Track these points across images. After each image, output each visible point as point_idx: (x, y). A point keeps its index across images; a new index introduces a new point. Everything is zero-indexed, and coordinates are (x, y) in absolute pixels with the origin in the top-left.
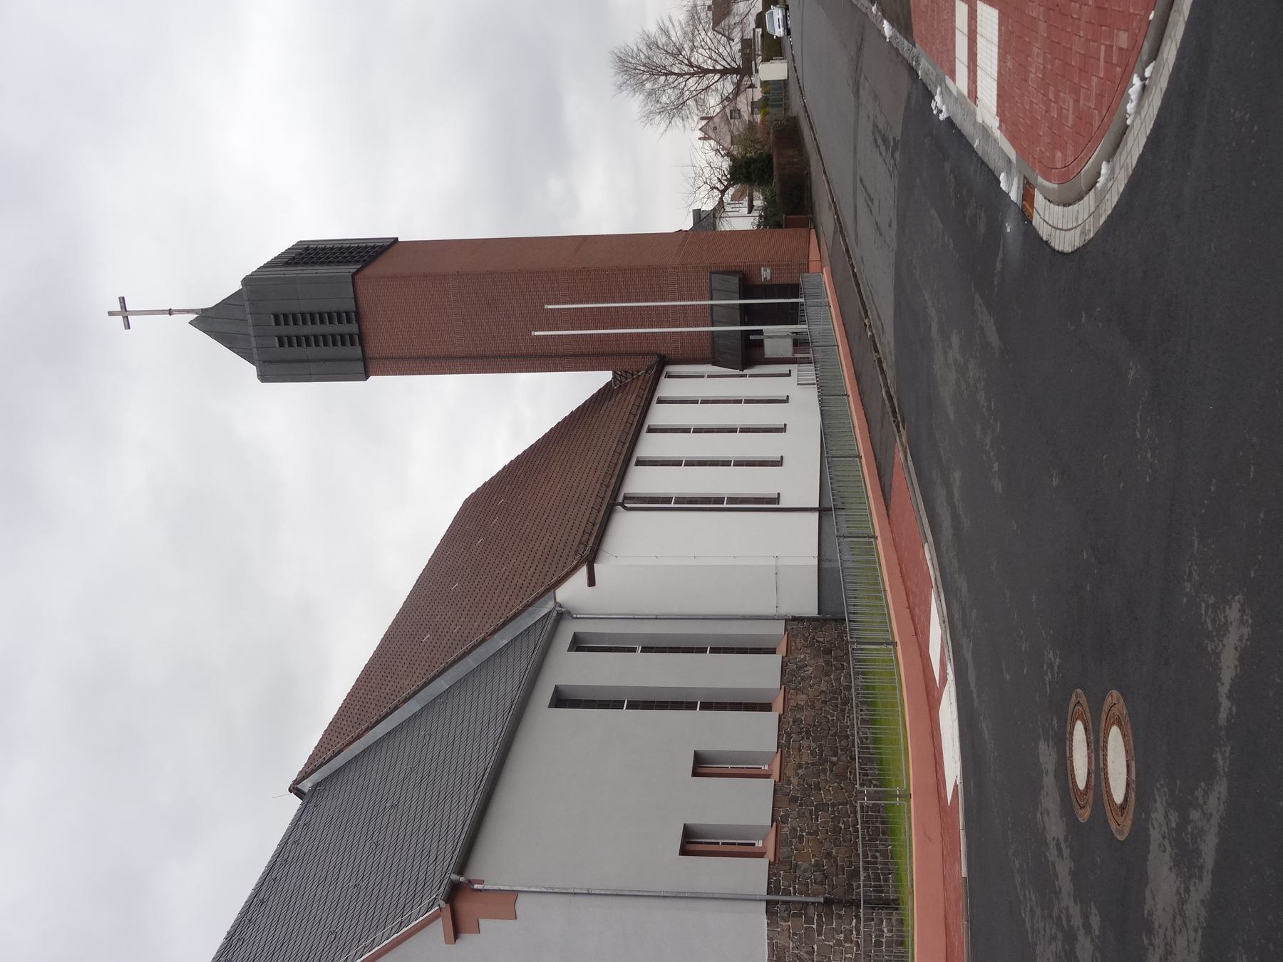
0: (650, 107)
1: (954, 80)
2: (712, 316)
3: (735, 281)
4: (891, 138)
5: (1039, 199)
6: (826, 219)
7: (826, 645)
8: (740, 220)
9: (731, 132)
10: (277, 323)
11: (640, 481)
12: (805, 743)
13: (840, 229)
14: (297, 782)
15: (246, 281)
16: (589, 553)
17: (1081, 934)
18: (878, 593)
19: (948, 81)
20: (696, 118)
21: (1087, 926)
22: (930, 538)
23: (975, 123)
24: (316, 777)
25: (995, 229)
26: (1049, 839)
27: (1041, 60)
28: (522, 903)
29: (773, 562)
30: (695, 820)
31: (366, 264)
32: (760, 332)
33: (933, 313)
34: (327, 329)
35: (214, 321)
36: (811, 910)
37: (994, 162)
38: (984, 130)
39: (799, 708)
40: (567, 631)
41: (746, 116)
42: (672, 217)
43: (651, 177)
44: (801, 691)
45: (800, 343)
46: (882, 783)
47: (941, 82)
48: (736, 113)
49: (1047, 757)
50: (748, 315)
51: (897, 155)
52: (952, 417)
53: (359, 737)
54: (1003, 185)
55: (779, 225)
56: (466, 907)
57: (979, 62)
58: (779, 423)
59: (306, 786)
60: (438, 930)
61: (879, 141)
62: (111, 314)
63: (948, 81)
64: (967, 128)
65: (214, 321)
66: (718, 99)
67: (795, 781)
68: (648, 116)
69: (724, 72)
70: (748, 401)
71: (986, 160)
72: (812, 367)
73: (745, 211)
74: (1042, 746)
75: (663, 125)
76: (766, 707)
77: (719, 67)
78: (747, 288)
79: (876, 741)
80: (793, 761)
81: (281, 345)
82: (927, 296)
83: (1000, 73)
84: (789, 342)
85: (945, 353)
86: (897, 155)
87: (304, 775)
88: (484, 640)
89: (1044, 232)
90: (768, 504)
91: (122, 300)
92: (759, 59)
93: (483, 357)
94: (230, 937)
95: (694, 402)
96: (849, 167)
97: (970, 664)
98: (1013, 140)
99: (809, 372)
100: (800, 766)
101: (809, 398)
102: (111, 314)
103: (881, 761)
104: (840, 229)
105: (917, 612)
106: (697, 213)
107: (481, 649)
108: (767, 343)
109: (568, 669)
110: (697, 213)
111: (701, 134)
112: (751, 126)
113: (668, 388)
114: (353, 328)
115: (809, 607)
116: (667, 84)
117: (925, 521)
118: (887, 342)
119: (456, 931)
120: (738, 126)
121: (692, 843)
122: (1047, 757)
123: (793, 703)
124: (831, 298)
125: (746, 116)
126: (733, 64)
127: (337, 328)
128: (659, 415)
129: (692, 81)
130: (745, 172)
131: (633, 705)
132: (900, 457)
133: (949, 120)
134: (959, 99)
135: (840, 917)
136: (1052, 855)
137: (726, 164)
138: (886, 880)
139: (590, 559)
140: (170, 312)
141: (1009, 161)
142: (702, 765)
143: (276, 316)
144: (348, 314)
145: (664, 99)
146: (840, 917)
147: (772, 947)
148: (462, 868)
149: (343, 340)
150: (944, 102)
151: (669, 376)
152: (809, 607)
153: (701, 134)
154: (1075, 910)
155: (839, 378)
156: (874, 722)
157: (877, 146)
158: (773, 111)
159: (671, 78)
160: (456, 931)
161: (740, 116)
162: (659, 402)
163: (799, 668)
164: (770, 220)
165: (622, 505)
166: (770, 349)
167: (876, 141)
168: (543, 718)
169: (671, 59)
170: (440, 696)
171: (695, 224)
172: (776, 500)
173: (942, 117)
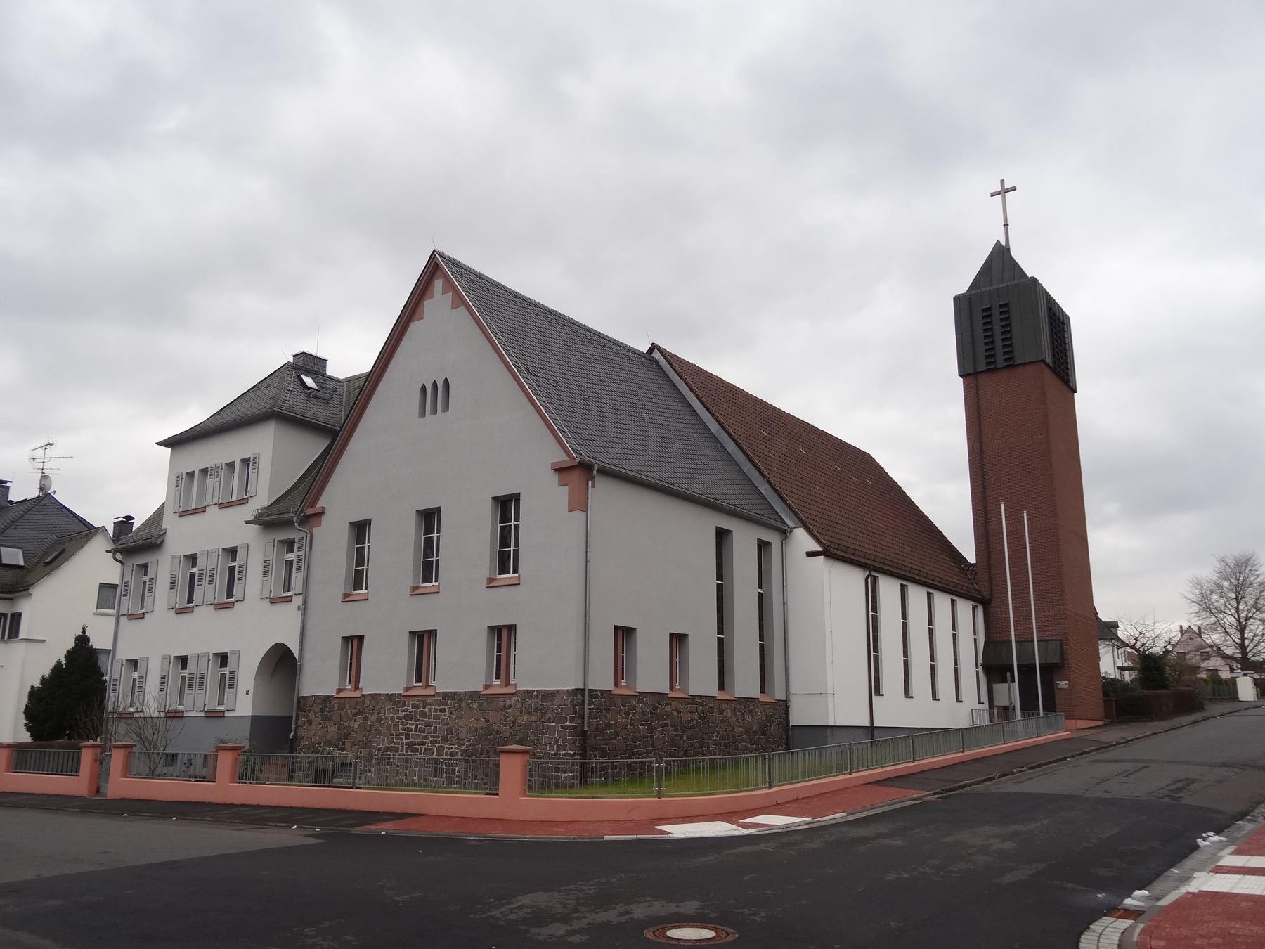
0: (1207, 586)
1: (1233, 853)
2: (1025, 642)
3: (1056, 660)
4: (1181, 795)
5: (1125, 924)
6: (1112, 735)
7: (765, 733)
8: (1109, 663)
9: (1189, 653)
10: (1001, 306)
11: (889, 589)
12: (696, 716)
13: (1104, 747)
14: (659, 348)
15: (1034, 280)
16: (831, 552)
17: (568, 928)
18: (809, 774)
19: (1232, 848)
20: (1199, 623)
21: (573, 932)
22: (851, 818)
23: (1194, 870)
24: (662, 361)
25: (1101, 885)
26: (633, 906)
27: (1246, 932)
28: (580, 515)
29: (830, 691)
30: (640, 636)
31: (1053, 370)
32: (1013, 681)
33: (1031, 826)
34: (998, 338)
35: (1001, 259)
36: (579, 721)
37: (1159, 886)
38: (1186, 879)
39: (721, 712)
40: (772, 537)
41: (1204, 665)
42: (1108, 602)
43: (1143, 586)
44: (734, 714)
45: (1006, 712)
46: (668, 773)
47: (1232, 841)
48: (1207, 656)
49: (690, 907)
50: (1027, 670)
51: (1167, 800)
52: (945, 840)
53: (692, 390)
54: (1137, 893)
55: (1105, 694)
56: (576, 476)
57: (1248, 877)
58: (940, 695)
59: (656, 355)
60: (561, 457)
61: (1180, 784)
62: (1002, 181)
63: (1232, 848)
64: (1189, 863)
65: (1001, 259)
66: (1217, 642)
67: (669, 708)
68: (1197, 583)
69: (1242, 647)
70: (956, 670)
71: (1161, 879)
72: (987, 723)
73: (1120, 665)
74: (697, 904)
75: (1191, 596)
76: (721, 687)
77: (1247, 642)
78: (1050, 671)
79: (698, 769)
80: (682, 707)
81: (984, 310)
82: (1045, 822)
83: (1236, 895)
84: (1007, 704)
85: (997, 837)
86: (1167, 800)
87: (664, 353)
88: (763, 476)
89: (1097, 927)
90: (875, 687)
91: (1014, 189)
92: (1257, 676)
93: (982, 463)
94: (553, 313)
95: (955, 627)
96: (1158, 757)
97: (757, 848)
98: (1177, 904)
99: (983, 720)
100: (679, 712)
101: (962, 721)
102: (1002, 181)
103: (683, 773)
104: (1104, 747)
105: (795, 805)
106: (1115, 625)
107: (757, 474)
108: (1006, 685)
109: (744, 540)
110: (1115, 625)
111: (1185, 628)
112: (1196, 669)
113: (964, 607)
114: (1000, 363)
115: (797, 719)
116: (1229, 599)
117: (864, 814)
118: (1008, 786)
119: (560, 470)
120: (1194, 659)
121: (624, 634)
122: (690, 907)
123: (724, 707)
124: (1044, 738)
125: (1204, 665)
126: (1250, 655)
127: (999, 351)
128: (942, 602)
129: (1232, 620)
130: (1150, 666)
131: (720, 588)
132: (914, 795)
133: (1197, 847)
134: (1215, 857)
135: (574, 742)
136: (621, 908)
137: (1158, 649)
138: (601, 776)
139: (828, 553)
140: (1006, 225)
141: (1159, 899)
142: (678, 640)
143: (1006, 305)
144: (1011, 359)
145: (1214, 597)
146: (574, 742)
147: (553, 693)
148: (604, 472)
149: (990, 356)
150: (1213, 843)
151: (974, 608)
152: (797, 719)
153: (1185, 628)
154: (583, 924)
155: (978, 745)
156: (712, 768)
157: (1175, 783)
158: (1210, 687)
159: (1234, 603)
160: (560, 470)
161: (1204, 660)
162: (953, 601)
163: (750, 711)
164: (1110, 687)
165: (870, 575)
166: (1000, 688)
167: (1180, 781)
168: (707, 524)
169: (1251, 602)
170: (722, 446)
171: (1106, 623)
172: (878, 693)
173: (1199, 841)
